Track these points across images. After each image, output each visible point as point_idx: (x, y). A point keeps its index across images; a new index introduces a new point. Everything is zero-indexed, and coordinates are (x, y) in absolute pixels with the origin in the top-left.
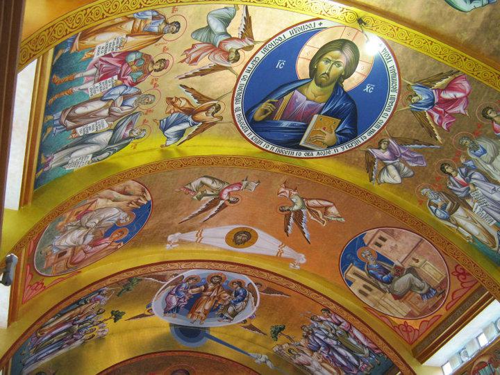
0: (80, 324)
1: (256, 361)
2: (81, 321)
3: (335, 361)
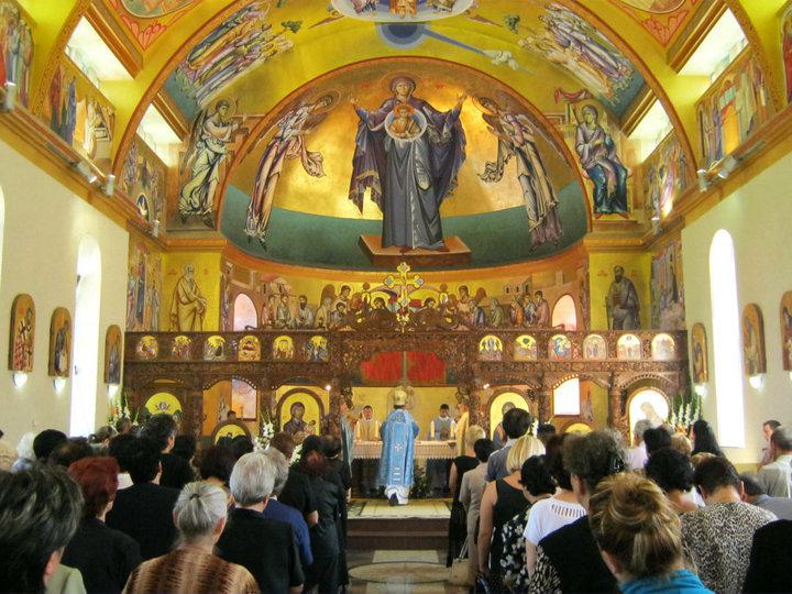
0: (246, 45)
1: (493, 62)
2: (245, 41)
3: (592, 61)
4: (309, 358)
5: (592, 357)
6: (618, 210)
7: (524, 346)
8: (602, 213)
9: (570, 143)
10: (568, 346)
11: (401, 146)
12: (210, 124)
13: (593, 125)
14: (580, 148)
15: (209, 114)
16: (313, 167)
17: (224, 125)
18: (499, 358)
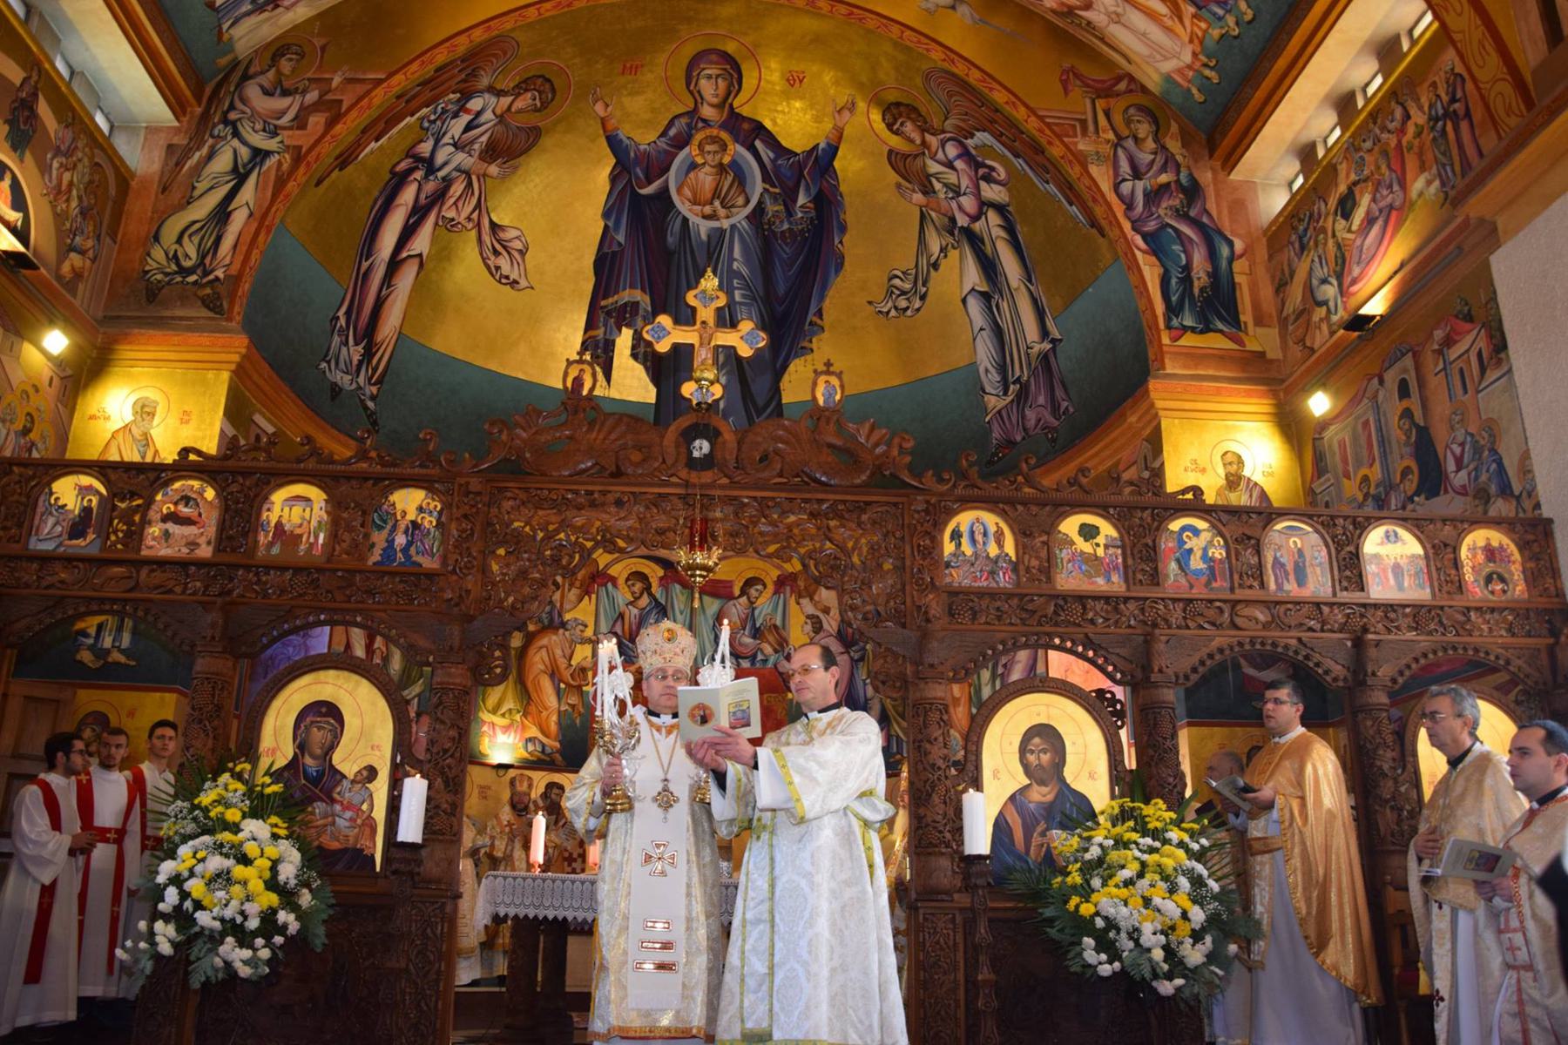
4: (375, 556)
5: (1291, 587)
6: (1220, 326)
7: (1083, 546)
8: (1185, 329)
9: (1101, 176)
10: (1218, 553)
11: (704, 237)
12: (252, 91)
13: (1150, 144)
14: (1126, 188)
15: (252, 70)
16: (504, 263)
17: (286, 93)
18: (1004, 580)
